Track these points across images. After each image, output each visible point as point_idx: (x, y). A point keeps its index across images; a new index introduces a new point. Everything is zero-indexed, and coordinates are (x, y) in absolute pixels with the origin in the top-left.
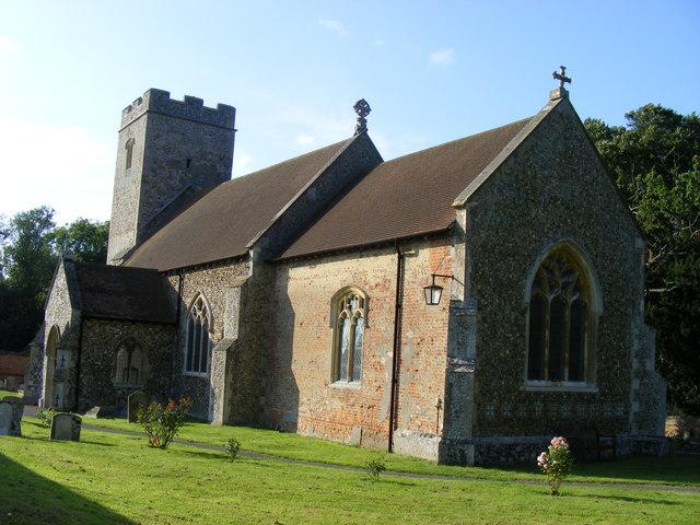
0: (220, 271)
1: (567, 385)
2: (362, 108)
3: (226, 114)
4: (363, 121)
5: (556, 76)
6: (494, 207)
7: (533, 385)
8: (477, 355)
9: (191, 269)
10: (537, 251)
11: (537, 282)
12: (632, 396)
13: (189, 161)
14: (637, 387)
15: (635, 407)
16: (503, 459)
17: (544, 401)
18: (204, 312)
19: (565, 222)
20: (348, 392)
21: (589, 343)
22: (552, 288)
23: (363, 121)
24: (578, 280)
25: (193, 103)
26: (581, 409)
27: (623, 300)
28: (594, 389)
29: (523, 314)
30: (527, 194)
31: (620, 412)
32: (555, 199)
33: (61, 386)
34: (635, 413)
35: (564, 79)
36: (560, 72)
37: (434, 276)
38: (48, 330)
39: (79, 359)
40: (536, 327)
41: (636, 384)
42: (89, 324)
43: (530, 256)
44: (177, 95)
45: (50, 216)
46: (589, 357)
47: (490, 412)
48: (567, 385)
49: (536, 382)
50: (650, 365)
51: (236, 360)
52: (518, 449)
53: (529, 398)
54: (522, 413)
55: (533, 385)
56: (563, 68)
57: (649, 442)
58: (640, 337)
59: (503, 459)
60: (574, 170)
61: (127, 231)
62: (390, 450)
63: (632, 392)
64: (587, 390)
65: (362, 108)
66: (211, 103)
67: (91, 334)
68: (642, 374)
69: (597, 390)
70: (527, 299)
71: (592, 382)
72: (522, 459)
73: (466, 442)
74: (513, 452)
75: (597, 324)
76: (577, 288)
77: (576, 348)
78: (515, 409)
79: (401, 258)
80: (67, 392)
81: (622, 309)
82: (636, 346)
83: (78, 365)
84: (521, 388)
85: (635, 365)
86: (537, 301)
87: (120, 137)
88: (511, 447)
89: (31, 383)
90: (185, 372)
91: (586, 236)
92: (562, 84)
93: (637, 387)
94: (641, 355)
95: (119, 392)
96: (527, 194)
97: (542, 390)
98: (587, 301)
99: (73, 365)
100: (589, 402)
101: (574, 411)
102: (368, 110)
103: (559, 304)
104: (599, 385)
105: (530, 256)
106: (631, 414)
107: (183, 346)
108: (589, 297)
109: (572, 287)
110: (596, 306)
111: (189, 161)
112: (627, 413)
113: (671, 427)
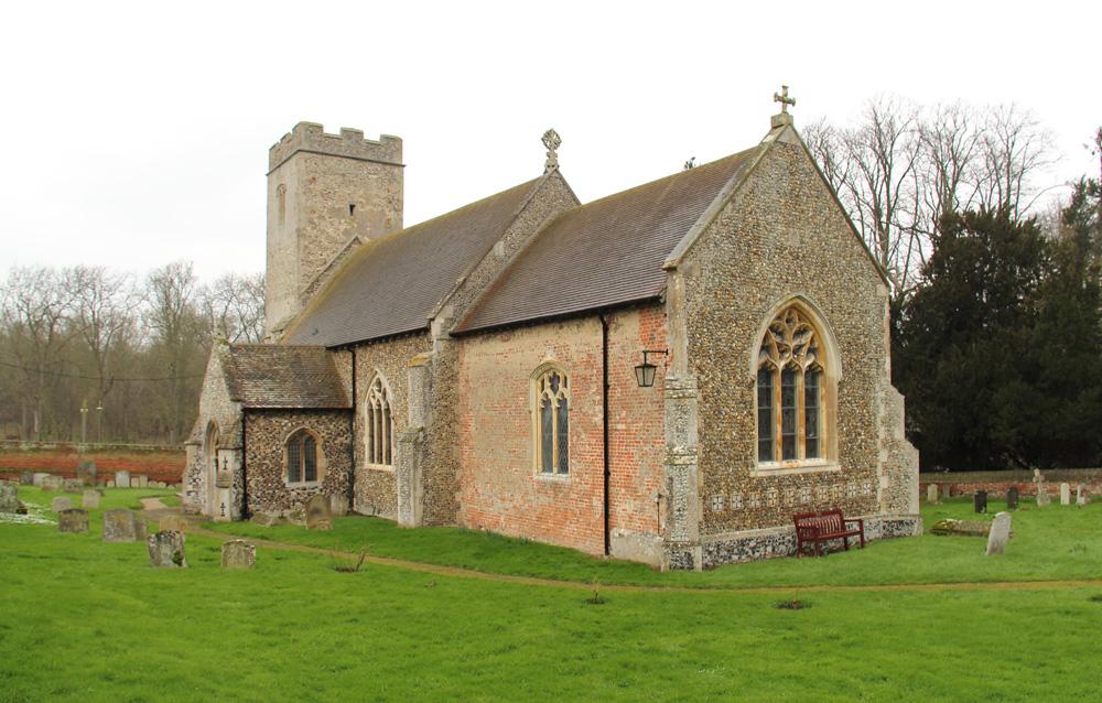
0: (400, 346)
1: (803, 463)
2: (551, 140)
3: (392, 144)
4: (552, 156)
5: (777, 98)
6: (711, 266)
7: (763, 468)
8: (701, 441)
9: (364, 344)
10: (763, 312)
11: (765, 348)
12: (880, 470)
13: (352, 207)
14: (885, 459)
15: (884, 483)
16: (735, 557)
17: (780, 487)
18: (385, 394)
19: (795, 274)
20: (556, 486)
21: (828, 414)
22: (782, 352)
23: (552, 156)
24: (812, 341)
25: (352, 135)
26: (821, 490)
27: (865, 360)
28: (836, 467)
29: (750, 387)
30: (749, 246)
31: (866, 492)
32: (782, 249)
33: (226, 492)
34: (884, 490)
35: (785, 100)
36: (780, 94)
37: (645, 352)
38: (203, 424)
39: (244, 458)
40: (765, 396)
41: (883, 456)
42: (252, 417)
43: (755, 320)
44: (332, 129)
45: (189, 270)
46: (828, 430)
47: (718, 507)
48: (803, 463)
49: (768, 465)
50: (899, 433)
51: (426, 454)
52: (752, 544)
53: (760, 485)
54: (755, 503)
55: (763, 468)
56: (785, 88)
57: (901, 522)
58: (887, 402)
59: (735, 557)
60: (803, 211)
61: (286, 296)
62: (607, 552)
63: (879, 465)
64: (829, 469)
65: (551, 140)
66: (372, 135)
67: (256, 429)
68: (891, 444)
69: (839, 468)
70: (754, 371)
71: (833, 459)
72: (757, 554)
73: (693, 544)
74: (746, 549)
75: (837, 390)
76: (812, 351)
77: (811, 424)
78: (745, 499)
79: (606, 330)
80: (234, 500)
81: (865, 370)
82: (882, 412)
83: (244, 467)
84: (752, 474)
85: (882, 433)
86: (766, 372)
87: (269, 182)
88: (743, 543)
89: (190, 488)
90: (367, 465)
91: (820, 289)
92: (784, 107)
93: (885, 459)
94: (888, 422)
95: (294, 493)
96: (749, 246)
97: (777, 473)
98: (823, 365)
99: (238, 466)
100: (830, 482)
101: (814, 494)
102: (557, 144)
103: (789, 373)
104: (841, 461)
105: (755, 320)
106: (880, 491)
107: (362, 435)
108: (825, 360)
109: (805, 349)
110: (834, 369)
111: (352, 207)
112: (874, 490)
113: (985, 325)
